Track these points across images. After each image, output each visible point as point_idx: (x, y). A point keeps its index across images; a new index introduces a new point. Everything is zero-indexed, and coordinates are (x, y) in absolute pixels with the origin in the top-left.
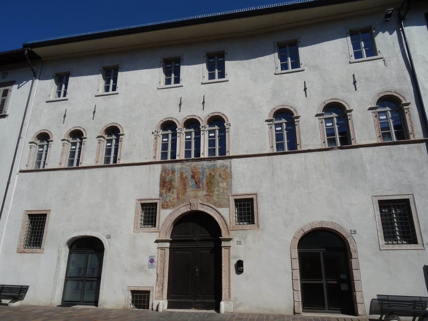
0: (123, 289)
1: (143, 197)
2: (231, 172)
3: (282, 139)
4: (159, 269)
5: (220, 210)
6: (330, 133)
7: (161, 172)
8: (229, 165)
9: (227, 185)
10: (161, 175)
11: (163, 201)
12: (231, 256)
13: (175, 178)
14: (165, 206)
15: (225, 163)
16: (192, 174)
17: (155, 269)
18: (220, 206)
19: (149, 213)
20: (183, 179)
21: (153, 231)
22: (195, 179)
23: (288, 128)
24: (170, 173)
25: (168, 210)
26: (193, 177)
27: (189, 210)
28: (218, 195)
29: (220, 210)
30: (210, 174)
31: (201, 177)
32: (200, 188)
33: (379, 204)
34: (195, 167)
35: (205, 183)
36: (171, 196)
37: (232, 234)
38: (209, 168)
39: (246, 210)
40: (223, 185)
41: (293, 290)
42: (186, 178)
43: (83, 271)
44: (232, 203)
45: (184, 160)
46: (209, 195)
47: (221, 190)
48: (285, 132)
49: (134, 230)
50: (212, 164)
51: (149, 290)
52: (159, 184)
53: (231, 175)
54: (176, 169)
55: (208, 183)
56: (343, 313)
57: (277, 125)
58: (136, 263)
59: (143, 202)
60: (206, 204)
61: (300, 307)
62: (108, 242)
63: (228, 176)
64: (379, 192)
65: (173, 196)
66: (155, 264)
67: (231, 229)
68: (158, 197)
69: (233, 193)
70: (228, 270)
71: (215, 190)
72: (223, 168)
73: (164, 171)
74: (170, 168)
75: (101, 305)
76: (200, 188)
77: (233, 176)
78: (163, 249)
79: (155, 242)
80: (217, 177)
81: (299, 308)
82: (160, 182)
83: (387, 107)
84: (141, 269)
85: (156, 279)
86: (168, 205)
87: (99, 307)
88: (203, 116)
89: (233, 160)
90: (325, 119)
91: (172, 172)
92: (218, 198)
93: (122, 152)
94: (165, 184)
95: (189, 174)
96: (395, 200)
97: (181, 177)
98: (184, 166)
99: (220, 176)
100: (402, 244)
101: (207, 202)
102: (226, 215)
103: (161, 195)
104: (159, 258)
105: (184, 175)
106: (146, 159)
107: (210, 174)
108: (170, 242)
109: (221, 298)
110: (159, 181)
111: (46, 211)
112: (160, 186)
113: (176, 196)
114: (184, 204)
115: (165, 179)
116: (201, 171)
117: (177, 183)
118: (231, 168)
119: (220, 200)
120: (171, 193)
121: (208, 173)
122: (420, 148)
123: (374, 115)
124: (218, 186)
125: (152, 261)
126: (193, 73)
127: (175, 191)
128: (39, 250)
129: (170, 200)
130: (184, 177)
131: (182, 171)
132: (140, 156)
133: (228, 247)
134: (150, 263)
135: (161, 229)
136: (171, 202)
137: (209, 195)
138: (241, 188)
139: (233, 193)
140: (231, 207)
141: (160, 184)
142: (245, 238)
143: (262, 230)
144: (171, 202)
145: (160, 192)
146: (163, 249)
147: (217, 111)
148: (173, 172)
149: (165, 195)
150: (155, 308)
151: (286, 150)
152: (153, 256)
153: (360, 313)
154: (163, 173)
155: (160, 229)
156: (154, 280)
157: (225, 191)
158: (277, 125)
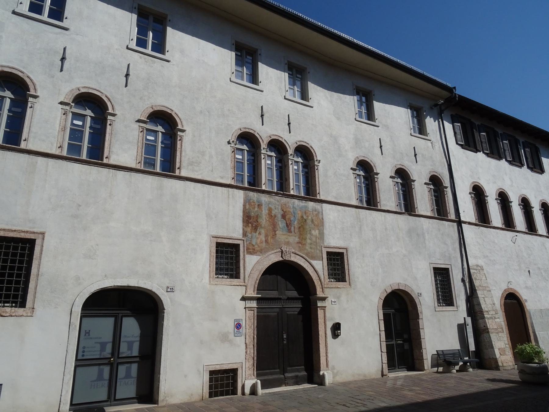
0: (198, 371)
1: (220, 234)
2: (323, 219)
3: (81, 139)
4: (247, 337)
5: (314, 262)
6: (76, 134)
7: (244, 202)
8: (320, 210)
9: (319, 233)
10: (244, 206)
11: (248, 243)
12: (327, 318)
13: (261, 214)
14: (251, 251)
15: (316, 207)
16: (282, 213)
17: (243, 338)
18: (314, 258)
19: (227, 259)
20: (271, 217)
21: (238, 284)
22: (285, 220)
23: (13, 109)
24: (256, 206)
25: (255, 257)
26: (284, 217)
27: (281, 259)
28: (311, 244)
29: (314, 262)
30: (302, 217)
31: (292, 219)
32: (291, 232)
33: (216, 247)
34: (286, 205)
35: (296, 227)
36: (257, 238)
37: (328, 293)
38: (301, 208)
39: (337, 264)
40: (315, 232)
41: (382, 352)
42: (275, 216)
43: (109, 348)
44: (325, 256)
45: (274, 193)
46: (301, 243)
47: (314, 239)
48: (87, 131)
49: (210, 281)
50: (303, 204)
51: (236, 367)
52: (241, 219)
53: (323, 223)
54: (263, 202)
55: (300, 228)
56: (409, 369)
57: (76, 116)
58: (208, 331)
59: (220, 241)
60: (299, 253)
61: (70, 379)
62: (170, 299)
63: (320, 224)
64: (434, 260)
65: (259, 238)
66: (243, 330)
67: (326, 286)
68: (241, 237)
69: (325, 244)
70: (324, 335)
71: (308, 238)
72: (315, 213)
73: (247, 201)
74: (255, 199)
75: (163, 400)
76: (291, 232)
77: (325, 223)
78: (252, 309)
79: (241, 300)
80: (309, 222)
81: (386, 371)
82: (243, 215)
83: (245, 146)
84: (224, 338)
85: (245, 351)
86: (254, 249)
87: (161, 404)
88: (291, 141)
89: (325, 205)
90: (74, 114)
91: (258, 205)
92: (311, 248)
93: (183, 159)
94: (250, 219)
95: (278, 212)
96: (224, 243)
97: (269, 214)
98: (272, 200)
99: (312, 221)
100: (443, 306)
101: (300, 251)
102: (318, 268)
103: (245, 234)
104: (247, 322)
105: (273, 212)
106: (222, 178)
107: (302, 217)
108: (258, 299)
109: (320, 367)
110: (242, 214)
111: (34, 233)
112: (243, 222)
113: (264, 239)
114: (275, 251)
115: (249, 212)
116: (292, 210)
117: (264, 220)
118: (322, 214)
119: (313, 251)
120: (257, 233)
121: (300, 215)
122: (453, 226)
123: (141, 130)
124: (310, 233)
125: (238, 326)
126: (273, 79)
127: (263, 231)
128: (20, 311)
129: (256, 243)
130: (273, 215)
131: (270, 206)
132: (212, 171)
133: (324, 308)
134: (236, 330)
135: (248, 282)
136: (258, 246)
137: (301, 243)
138: (334, 240)
139: (325, 244)
140: (324, 260)
141: (243, 219)
142: (339, 298)
143: (354, 289)
144: (258, 246)
145: (243, 230)
146: (252, 309)
147: (305, 140)
148: (260, 206)
149: (250, 235)
150: (247, 391)
151: (84, 156)
152: (239, 320)
153: (426, 368)
154: (247, 204)
155: (246, 281)
156: (238, 354)
157: (317, 240)
158: (76, 116)
